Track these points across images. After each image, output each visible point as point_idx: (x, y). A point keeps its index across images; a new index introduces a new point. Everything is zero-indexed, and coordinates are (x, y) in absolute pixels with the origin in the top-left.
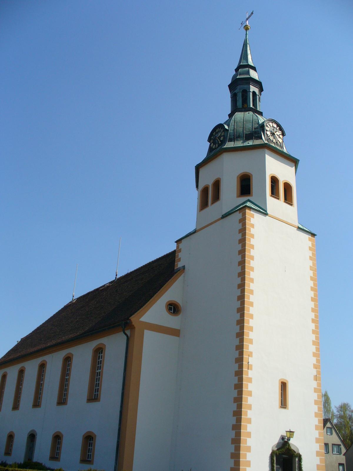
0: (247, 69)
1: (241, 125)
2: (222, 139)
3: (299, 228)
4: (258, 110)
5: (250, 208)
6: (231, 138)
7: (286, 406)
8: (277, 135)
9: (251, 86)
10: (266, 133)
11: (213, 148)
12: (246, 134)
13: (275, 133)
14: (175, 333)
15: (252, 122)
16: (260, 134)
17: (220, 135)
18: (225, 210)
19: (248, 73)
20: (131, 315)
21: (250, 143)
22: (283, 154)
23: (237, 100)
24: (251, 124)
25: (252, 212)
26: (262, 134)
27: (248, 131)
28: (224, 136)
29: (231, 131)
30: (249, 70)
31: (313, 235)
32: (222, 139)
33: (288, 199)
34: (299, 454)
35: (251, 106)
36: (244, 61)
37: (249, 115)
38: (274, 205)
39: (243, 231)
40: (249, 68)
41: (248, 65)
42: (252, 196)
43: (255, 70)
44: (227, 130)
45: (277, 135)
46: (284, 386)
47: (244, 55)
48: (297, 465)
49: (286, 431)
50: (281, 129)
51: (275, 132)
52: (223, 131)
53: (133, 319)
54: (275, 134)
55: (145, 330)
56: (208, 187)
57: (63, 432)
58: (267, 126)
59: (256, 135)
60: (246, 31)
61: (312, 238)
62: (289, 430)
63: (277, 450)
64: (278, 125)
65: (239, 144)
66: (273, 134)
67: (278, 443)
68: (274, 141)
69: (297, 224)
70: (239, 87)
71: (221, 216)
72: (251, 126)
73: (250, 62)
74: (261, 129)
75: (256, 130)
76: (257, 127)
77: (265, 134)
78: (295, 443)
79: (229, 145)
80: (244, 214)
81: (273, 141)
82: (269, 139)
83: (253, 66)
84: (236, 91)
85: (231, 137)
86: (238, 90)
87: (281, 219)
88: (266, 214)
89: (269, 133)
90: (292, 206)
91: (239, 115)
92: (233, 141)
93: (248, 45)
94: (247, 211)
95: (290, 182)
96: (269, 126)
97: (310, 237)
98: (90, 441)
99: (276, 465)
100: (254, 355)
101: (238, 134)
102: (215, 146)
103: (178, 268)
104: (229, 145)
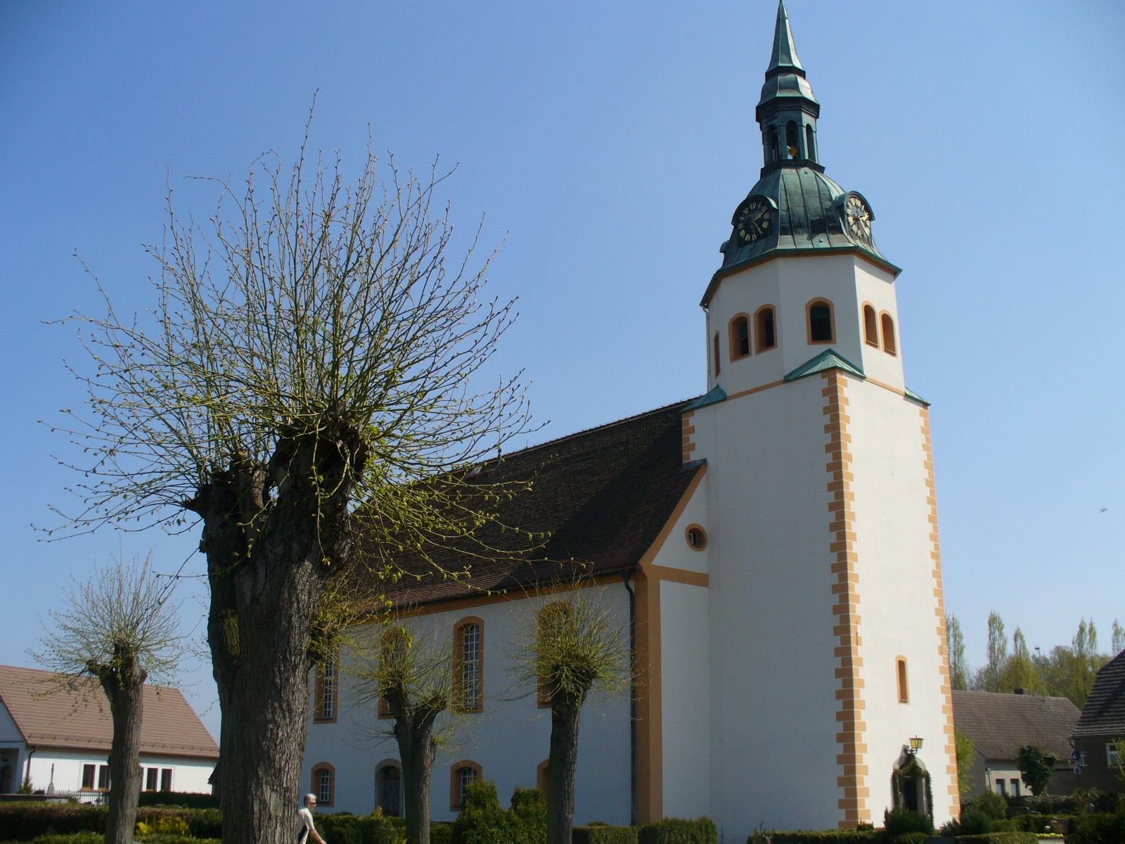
0: (792, 76)
1: (798, 199)
2: (765, 225)
3: (907, 397)
4: (817, 163)
5: (842, 370)
6: (785, 227)
7: (877, 343)
9: (803, 114)
10: (848, 220)
12: (812, 221)
14: (701, 580)
15: (818, 195)
18: (789, 368)
19: (795, 86)
20: (639, 558)
21: (822, 242)
24: (818, 199)
25: (844, 377)
26: (841, 222)
27: (814, 214)
28: (769, 220)
30: (796, 79)
31: (925, 405)
32: (765, 225)
33: (890, 348)
34: (927, 772)
35: (807, 157)
36: (784, 57)
38: (872, 357)
40: (794, 73)
42: (835, 343)
43: (804, 76)
45: (863, 221)
46: (902, 665)
47: (780, 45)
49: (911, 739)
50: (867, 209)
52: (767, 211)
53: (642, 562)
54: (859, 220)
55: (662, 582)
56: (746, 319)
57: (333, 762)
58: (848, 206)
63: (901, 768)
64: (864, 202)
66: (856, 220)
67: (901, 758)
69: (903, 390)
72: (818, 205)
73: (797, 64)
74: (838, 211)
75: (829, 213)
76: (830, 207)
78: (922, 757)
79: (785, 243)
80: (833, 381)
81: (857, 234)
83: (801, 68)
84: (775, 122)
85: (784, 225)
86: (780, 121)
88: (862, 378)
89: (851, 219)
91: (788, 175)
92: (789, 232)
93: (787, 21)
94: (838, 375)
96: (851, 206)
97: (922, 409)
99: (1119, 768)
100: (862, 620)
102: (751, 237)
104: (785, 243)
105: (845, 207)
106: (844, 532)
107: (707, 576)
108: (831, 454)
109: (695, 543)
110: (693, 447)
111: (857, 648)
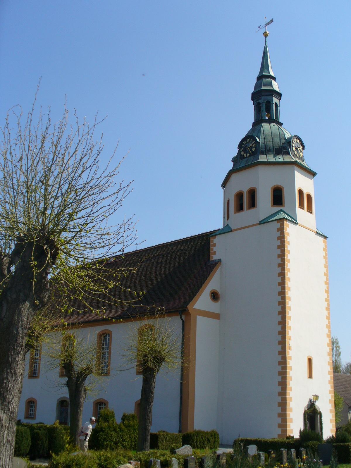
2: (253, 149)
3: (317, 233)
4: (279, 121)
5: (287, 219)
7: (312, 377)
8: (300, 150)
9: (274, 98)
10: (292, 149)
11: (244, 156)
12: (276, 149)
13: (298, 148)
14: (216, 316)
16: (288, 150)
17: (251, 146)
19: (271, 84)
21: (280, 158)
22: (303, 167)
23: (262, 110)
24: (279, 138)
28: (255, 147)
29: (262, 144)
30: (271, 81)
31: (326, 237)
32: (253, 149)
33: (310, 210)
34: (321, 412)
35: (275, 118)
37: (274, 126)
38: (301, 214)
39: (282, 238)
41: (270, 75)
44: (259, 143)
45: (300, 150)
46: (310, 360)
48: (319, 420)
49: (313, 396)
50: (302, 144)
51: (299, 147)
52: (255, 143)
56: (242, 193)
58: (293, 142)
59: (285, 151)
60: (266, 38)
61: (325, 240)
62: (315, 395)
65: (271, 158)
66: (297, 149)
67: (308, 405)
68: (298, 155)
69: (315, 230)
70: (263, 98)
71: (259, 222)
72: (279, 141)
73: (272, 74)
75: (284, 145)
76: (285, 142)
77: (292, 150)
79: (263, 158)
80: (282, 225)
82: (294, 154)
84: (260, 101)
87: (306, 227)
88: (296, 224)
90: (312, 214)
91: (266, 127)
93: (268, 53)
94: (285, 222)
95: (311, 193)
97: (324, 239)
98: (31, 404)
101: (269, 148)
102: (247, 155)
103: (213, 261)
105: (292, 143)
106: (285, 306)
107: (219, 314)
108: (280, 278)
109: (214, 299)
110: (215, 253)
111: (289, 351)
